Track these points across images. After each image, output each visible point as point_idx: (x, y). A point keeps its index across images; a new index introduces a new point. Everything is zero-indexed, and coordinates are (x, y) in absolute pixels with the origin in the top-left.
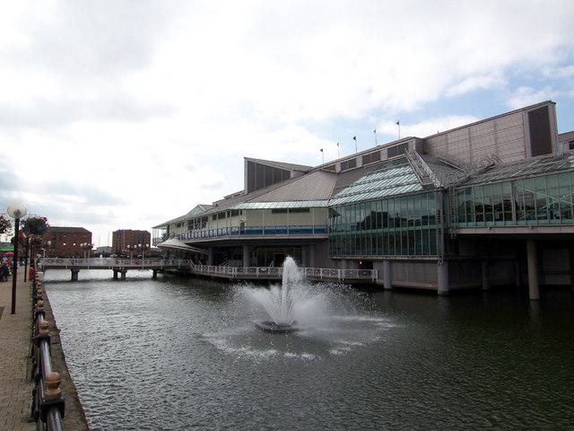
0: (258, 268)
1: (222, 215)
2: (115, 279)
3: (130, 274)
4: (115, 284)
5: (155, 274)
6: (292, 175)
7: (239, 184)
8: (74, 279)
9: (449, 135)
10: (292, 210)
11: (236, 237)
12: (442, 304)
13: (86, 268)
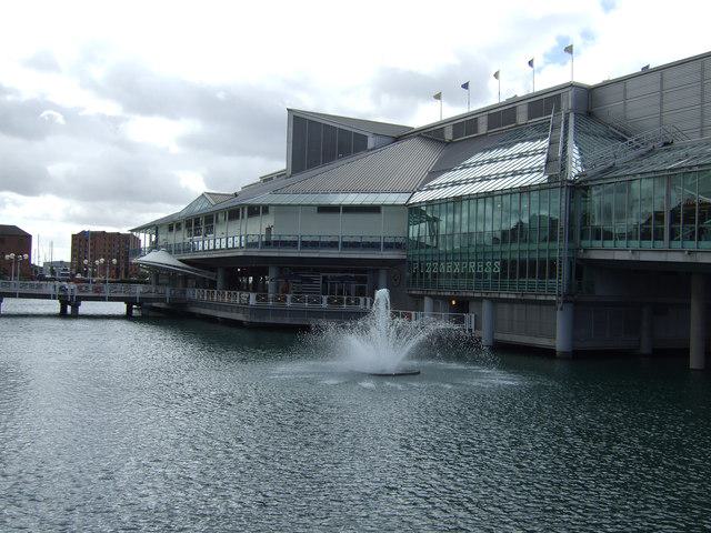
1: (233, 214)
2: (63, 315)
3: (86, 307)
4: (59, 323)
5: (129, 309)
6: (370, 144)
9: (629, 82)
10: (350, 209)
11: (255, 252)
13: (12, 295)
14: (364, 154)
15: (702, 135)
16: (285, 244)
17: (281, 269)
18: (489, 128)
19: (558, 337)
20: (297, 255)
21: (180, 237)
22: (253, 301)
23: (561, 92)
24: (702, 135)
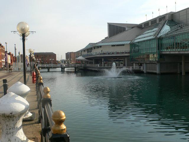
5: (75, 69)
6: (126, 30)
8: (49, 71)
17: (105, 59)
18: (159, 22)
19: (157, 70)
20: (124, 55)
22: (99, 66)
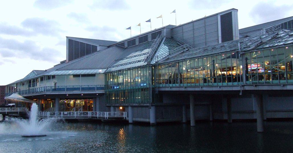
0: (62, 113)
6: (98, 49)
7: (62, 55)
10: (84, 75)
12: (152, 130)
14: (96, 53)
15: (206, 45)
16: (62, 90)
20: (50, 94)
21: (25, 88)
23: (134, 39)
24: (206, 45)
